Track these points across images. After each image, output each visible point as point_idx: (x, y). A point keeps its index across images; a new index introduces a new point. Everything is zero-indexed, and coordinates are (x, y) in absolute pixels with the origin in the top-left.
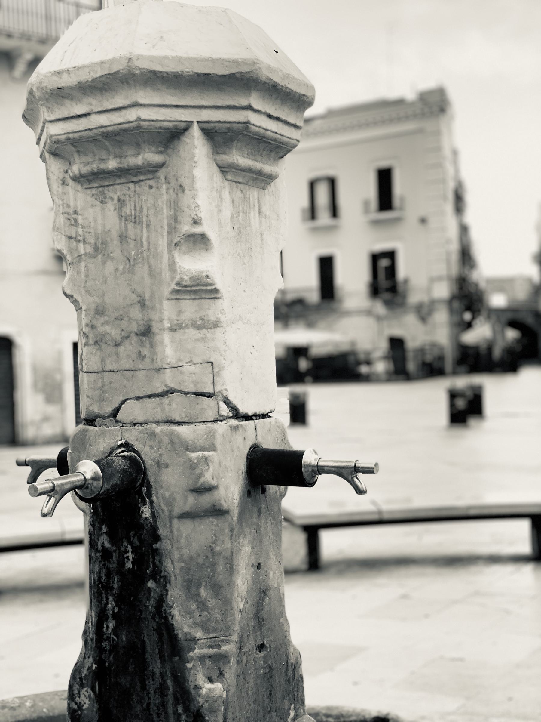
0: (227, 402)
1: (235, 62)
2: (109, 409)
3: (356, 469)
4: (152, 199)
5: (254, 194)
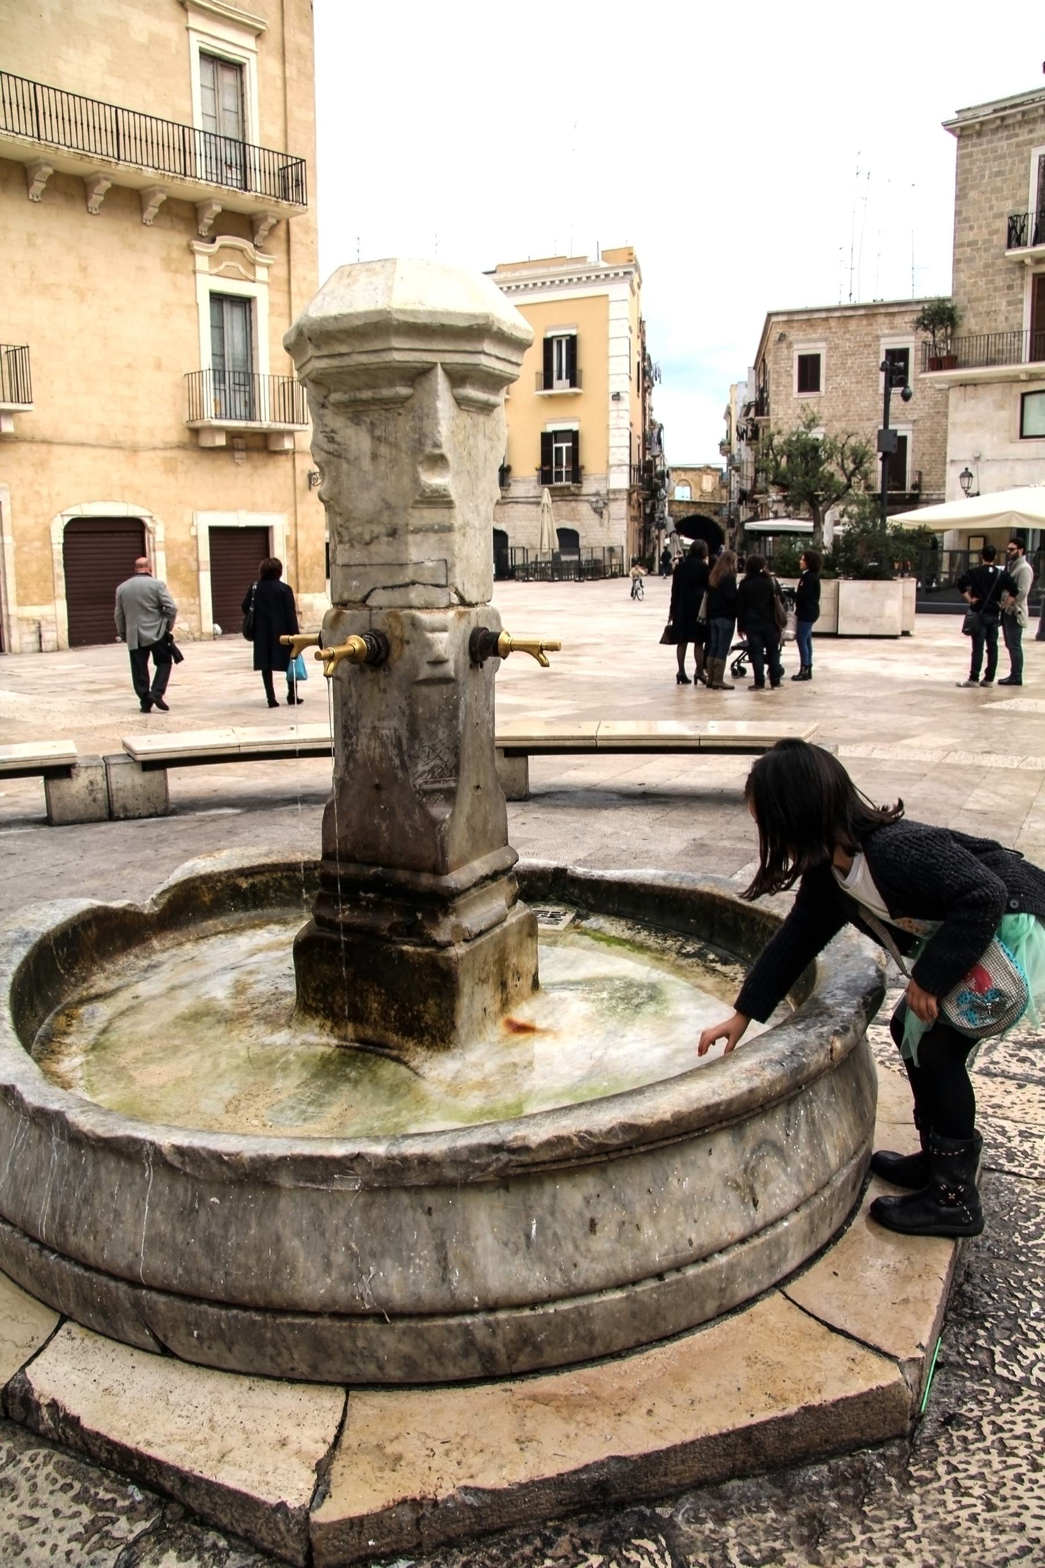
0: (457, 593)
1: (474, 316)
2: (359, 597)
3: (542, 649)
4: (402, 427)
5: (481, 418)
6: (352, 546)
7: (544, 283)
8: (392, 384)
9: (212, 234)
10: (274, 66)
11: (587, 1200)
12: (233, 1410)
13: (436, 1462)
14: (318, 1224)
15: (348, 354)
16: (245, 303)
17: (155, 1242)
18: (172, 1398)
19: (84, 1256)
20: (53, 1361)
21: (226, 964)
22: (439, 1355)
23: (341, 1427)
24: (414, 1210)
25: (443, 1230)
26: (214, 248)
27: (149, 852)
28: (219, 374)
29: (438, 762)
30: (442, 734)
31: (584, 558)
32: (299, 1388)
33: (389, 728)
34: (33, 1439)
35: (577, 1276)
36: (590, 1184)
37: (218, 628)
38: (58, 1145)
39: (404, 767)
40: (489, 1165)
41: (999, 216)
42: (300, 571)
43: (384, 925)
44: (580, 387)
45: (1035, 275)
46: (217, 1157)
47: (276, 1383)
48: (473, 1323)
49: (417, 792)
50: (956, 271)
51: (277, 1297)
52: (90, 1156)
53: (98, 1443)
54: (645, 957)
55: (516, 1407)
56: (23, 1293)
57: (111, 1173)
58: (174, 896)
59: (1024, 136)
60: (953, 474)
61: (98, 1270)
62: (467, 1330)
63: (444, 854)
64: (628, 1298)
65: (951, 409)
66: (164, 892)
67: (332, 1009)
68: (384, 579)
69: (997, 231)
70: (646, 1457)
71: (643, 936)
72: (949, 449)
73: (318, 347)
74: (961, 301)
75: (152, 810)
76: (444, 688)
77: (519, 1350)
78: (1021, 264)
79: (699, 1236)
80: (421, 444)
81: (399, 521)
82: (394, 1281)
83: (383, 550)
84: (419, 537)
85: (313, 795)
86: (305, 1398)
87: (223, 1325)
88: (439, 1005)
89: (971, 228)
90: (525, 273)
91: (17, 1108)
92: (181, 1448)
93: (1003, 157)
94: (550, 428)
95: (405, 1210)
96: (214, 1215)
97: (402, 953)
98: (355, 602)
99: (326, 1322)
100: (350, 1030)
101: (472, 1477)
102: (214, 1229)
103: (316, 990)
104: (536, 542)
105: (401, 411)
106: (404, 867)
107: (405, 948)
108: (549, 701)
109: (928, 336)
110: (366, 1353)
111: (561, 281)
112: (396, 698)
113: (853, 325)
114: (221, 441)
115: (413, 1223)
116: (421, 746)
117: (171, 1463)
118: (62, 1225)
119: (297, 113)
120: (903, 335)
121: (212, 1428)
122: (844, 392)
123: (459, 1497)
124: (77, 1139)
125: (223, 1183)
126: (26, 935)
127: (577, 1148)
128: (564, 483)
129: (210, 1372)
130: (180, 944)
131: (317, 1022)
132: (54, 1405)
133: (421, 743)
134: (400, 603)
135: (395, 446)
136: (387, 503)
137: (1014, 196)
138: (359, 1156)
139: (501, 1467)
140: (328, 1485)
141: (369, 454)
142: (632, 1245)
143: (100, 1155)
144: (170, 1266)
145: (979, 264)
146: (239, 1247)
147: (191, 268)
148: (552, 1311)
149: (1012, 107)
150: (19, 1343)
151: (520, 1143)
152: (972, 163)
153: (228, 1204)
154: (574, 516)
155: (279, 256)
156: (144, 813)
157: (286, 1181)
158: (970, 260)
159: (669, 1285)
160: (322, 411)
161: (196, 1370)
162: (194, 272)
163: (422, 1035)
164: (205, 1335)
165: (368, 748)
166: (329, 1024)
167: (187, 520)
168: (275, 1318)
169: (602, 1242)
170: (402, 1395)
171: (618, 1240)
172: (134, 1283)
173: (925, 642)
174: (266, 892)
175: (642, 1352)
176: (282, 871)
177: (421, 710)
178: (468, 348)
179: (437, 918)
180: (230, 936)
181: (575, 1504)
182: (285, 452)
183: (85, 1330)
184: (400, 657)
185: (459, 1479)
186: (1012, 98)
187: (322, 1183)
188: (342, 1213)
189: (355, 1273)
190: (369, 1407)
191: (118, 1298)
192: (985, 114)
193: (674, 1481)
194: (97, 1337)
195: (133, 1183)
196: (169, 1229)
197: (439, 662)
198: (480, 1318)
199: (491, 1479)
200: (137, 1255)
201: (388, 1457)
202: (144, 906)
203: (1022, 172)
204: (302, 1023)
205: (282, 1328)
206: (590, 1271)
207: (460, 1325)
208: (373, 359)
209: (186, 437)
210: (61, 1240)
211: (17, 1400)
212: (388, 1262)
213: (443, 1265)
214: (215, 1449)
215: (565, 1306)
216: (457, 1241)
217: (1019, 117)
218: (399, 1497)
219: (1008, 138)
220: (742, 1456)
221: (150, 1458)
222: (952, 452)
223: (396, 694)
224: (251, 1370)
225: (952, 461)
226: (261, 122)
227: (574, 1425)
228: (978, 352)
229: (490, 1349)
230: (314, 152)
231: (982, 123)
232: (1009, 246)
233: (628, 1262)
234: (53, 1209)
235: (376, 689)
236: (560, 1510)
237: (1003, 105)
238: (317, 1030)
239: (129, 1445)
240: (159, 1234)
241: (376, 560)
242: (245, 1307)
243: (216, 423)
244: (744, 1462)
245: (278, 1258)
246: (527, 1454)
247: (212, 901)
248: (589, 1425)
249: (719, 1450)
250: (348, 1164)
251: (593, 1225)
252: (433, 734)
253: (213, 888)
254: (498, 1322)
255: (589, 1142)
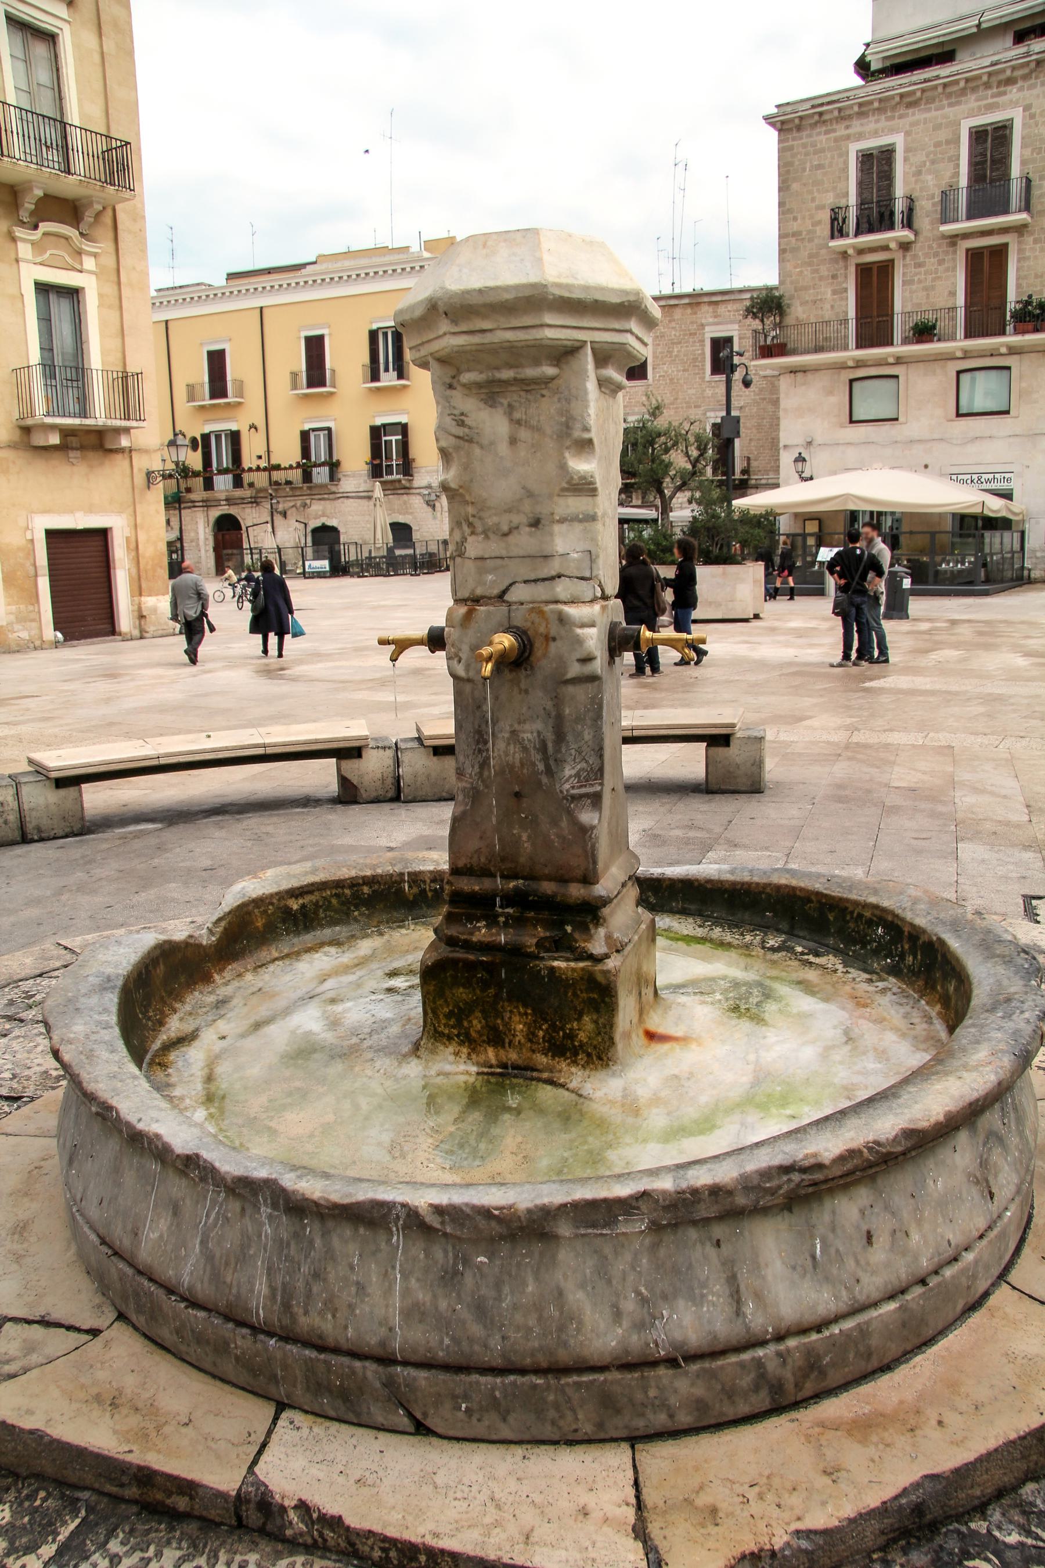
2: (496, 592)
6: (487, 537)
7: (332, 279)
8: (537, 363)
9: (34, 220)
10: (90, 39)
11: (862, 1212)
12: (512, 1485)
13: (755, 1507)
14: (603, 1271)
15: (490, 330)
16: (73, 294)
17: (413, 1312)
18: (440, 1479)
19: (320, 1337)
20: (282, 1456)
21: (299, 993)
22: (730, 1394)
23: (636, 1484)
24: (703, 1244)
25: (733, 1262)
26: (37, 235)
27: (80, 875)
28: (49, 368)
29: (584, 765)
30: (588, 735)
31: (418, 552)
32: (579, 1449)
33: (529, 733)
34: (280, 1547)
35: (861, 1292)
36: (863, 1195)
37: (59, 635)
38: (270, 1217)
39: (549, 772)
40: (780, 1187)
41: (821, 207)
42: (143, 574)
43: (529, 941)
44: (408, 379)
45: (857, 265)
46: (485, 1212)
47: (552, 1447)
48: (765, 1355)
49: (565, 798)
50: (782, 260)
51: (563, 1356)
52: (317, 1225)
53: (370, 1542)
54: (733, 954)
55: (808, 1437)
56: (218, 1383)
57: (347, 1244)
58: (229, 923)
59: (841, 131)
60: (786, 459)
61: (336, 1351)
62: (759, 1363)
63: (595, 863)
64: (900, 1307)
65: (782, 396)
66: (220, 920)
67: (467, 1035)
68: (525, 571)
69: (819, 222)
70: (957, 1471)
71: (717, 932)
72: (782, 435)
73: (455, 322)
74: (787, 290)
75: (68, 830)
76: (590, 687)
77: (806, 1376)
78: (844, 255)
79: (955, 1236)
80: (568, 427)
81: (543, 510)
82: (688, 1322)
83: (524, 541)
84: (564, 527)
85: (231, 804)
86: (588, 1459)
87: (497, 1394)
88: (596, 1022)
89: (795, 219)
90: (347, 264)
91: (203, 1179)
92: (475, 1534)
93: (822, 150)
94: (379, 421)
95: (694, 1245)
96: (482, 1276)
97: (552, 969)
98: (490, 598)
99: (615, 1375)
100: (491, 1054)
101: (799, 1519)
102: (483, 1291)
103: (449, 1015)
104: (369, 537)
105: (544, 392)
106: (549, 878)
107: (556, 963)
108: (433, 697)
109: (756, 324)
110: (657, 1402)
111: (376, 273)
112: (540, 699)
113: (678, 314)
114: (55, 439)
115: (703, 1259)
116: (568, 749)
117: (472, 1554)
118: (287, 1306)
119: (117, 92)
120: (727, 323)
121: (498, 1507)
122: (671, 380)
123: (795, 1542)
124: (297, 1208)
125: (492, 1240)
126: (109, 979)
127: (868, 1160)
128: (395, 477)
129: (475, 1445)
130: (240, 975)
131: (451, 1049)
132: (303, 1506)
133: (568, 746)
134: (544, 598)
135: (537, 429)
136: (528, 491)
137: (834, 188)
138: (645, 1194)
139: (824, 1503)
140: (657, 1552)
141: (506, 437)
142: (904, 1254)
143: (330, 1224)
144: (433, 1338)
145: (804, 254)
146: (515, 1307)
147: (13, 256)
148: (837, 1331)
149: (829, 103)
150: (236, 1441)
151: (812, 1161)
152: (793, 156)
153: (498, 1262)
154: (406, 510)
155: (107, 245)
156: (61, 833)
157: (565, 1229)
158: (795, 250)
159: (931, 1289)
160: (449, 392)
161: (457, 1445)
162: (17, 261)
163: (576, 1054)
164: (475, 1406)
165: (507, 755)
166: (465, 1050)
167: (22, 523)
168: (559, 1379)
169: (878, 1254)
170: (691, 1441)
171: (892, 1250)
172: (386, 1360)
173: (777, 624)
174: (316, 913)
175: (907, 1361)
176: (331, 888)
177: (567, 711)
178: (617, 326)
179: (588, 929)
180: (287, 962)
181: (895, 1531)
182: (121, 451)
183: (310, 1417)
184: (545, 655)
185: (788, 1524)
186: (828, 95)
187: (604, 1227)
188: (628, 1257)
189: (647, 1319)
190: (660, 1459)
191: (365, 1378)
192: (804, 109)
193: (978, 1493)
194: (328, 1423)
195: (378, 1250)
196: (428, 1298)
197: (588, 659)
198: (771, 1349)
199: (820, 1519)
200: (391, 1329)
201: (702, 1511)
202: (201, 936)
203: (841, 166)
204: (433, 1052)
205: (567, 1389)
206: (872, 1285)
207: (753, 1359)
208: (521, 335)
209: (16, 436)
210: (287, 1321)
211: (252, 1506)
212: (681, 1303)
213: (736, 1298)
214: (512, 1529)
215: (848, 1324)
216: (748, 1271)
217: (836, 113)
218: (737, 1553)
219: (827, 132)
220: (1035, 1457)
221: (442, 1551)
222: (786, 436)
223: (541, 694)
224: (527, 1437)
225: (785, 446)
226: (79, 100)
227: (872, 1448)
228: (806, 339)
229: (780, 1380)
230: (138, 134)
231: (801, 118)
232: (832, 237)
233: (902, 1271)
234: (273, 1289)
235: (516, 689)
236: (882, 1540)
237: (820, 101)
238: (452, 1058)
239: (413, 1539)
240: (416, 1305)
241: (515, 551)
242: (522, 1371)
243: (49, 420)
244: (1036, 1464)
245: (562, 1313)
246: (843, 1486)
247: (265, 926)
248: (888, 1445)
249: (1017, 1454)
250: (634, 1204)
251: (869, 1237)
252: (579, 736)
253: (265, 911)
254: (788, 1350)
255: (877, 1152)
